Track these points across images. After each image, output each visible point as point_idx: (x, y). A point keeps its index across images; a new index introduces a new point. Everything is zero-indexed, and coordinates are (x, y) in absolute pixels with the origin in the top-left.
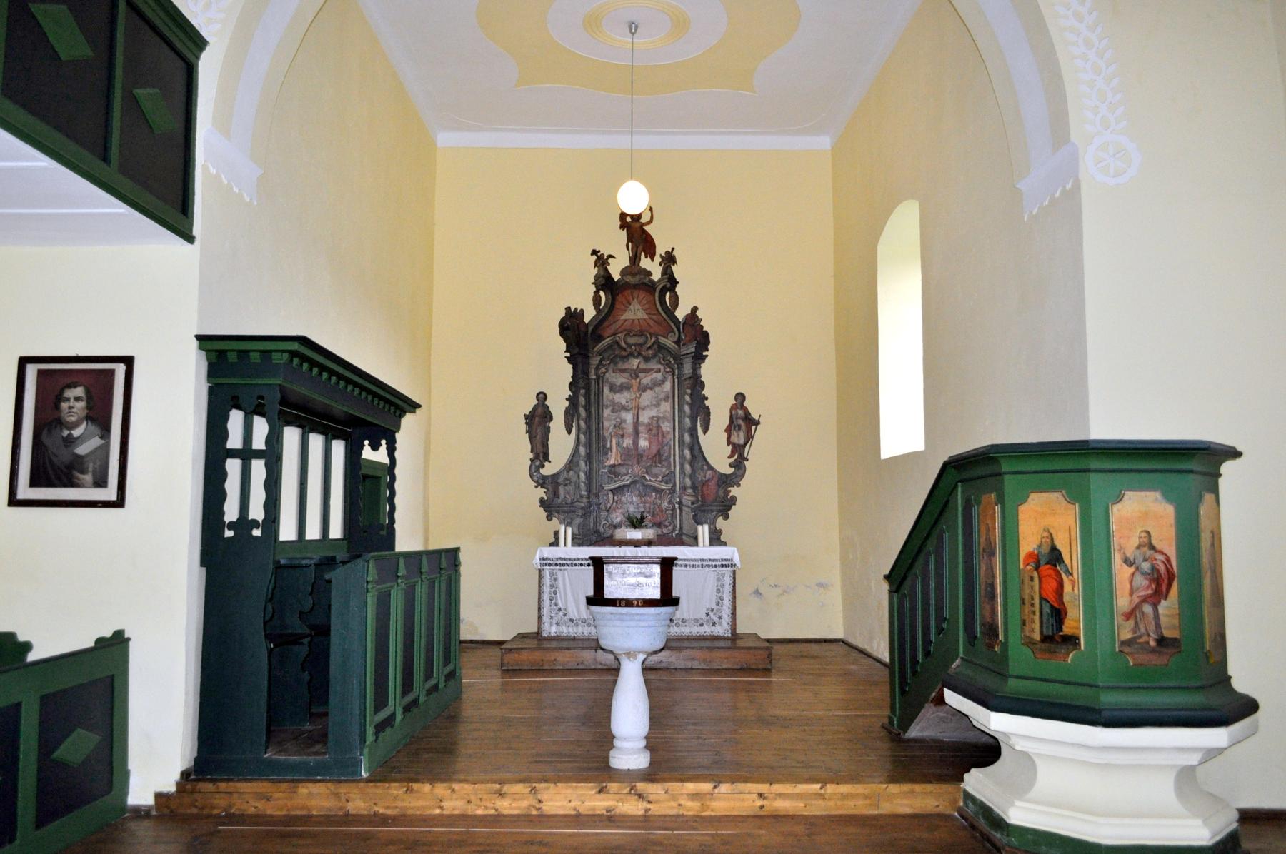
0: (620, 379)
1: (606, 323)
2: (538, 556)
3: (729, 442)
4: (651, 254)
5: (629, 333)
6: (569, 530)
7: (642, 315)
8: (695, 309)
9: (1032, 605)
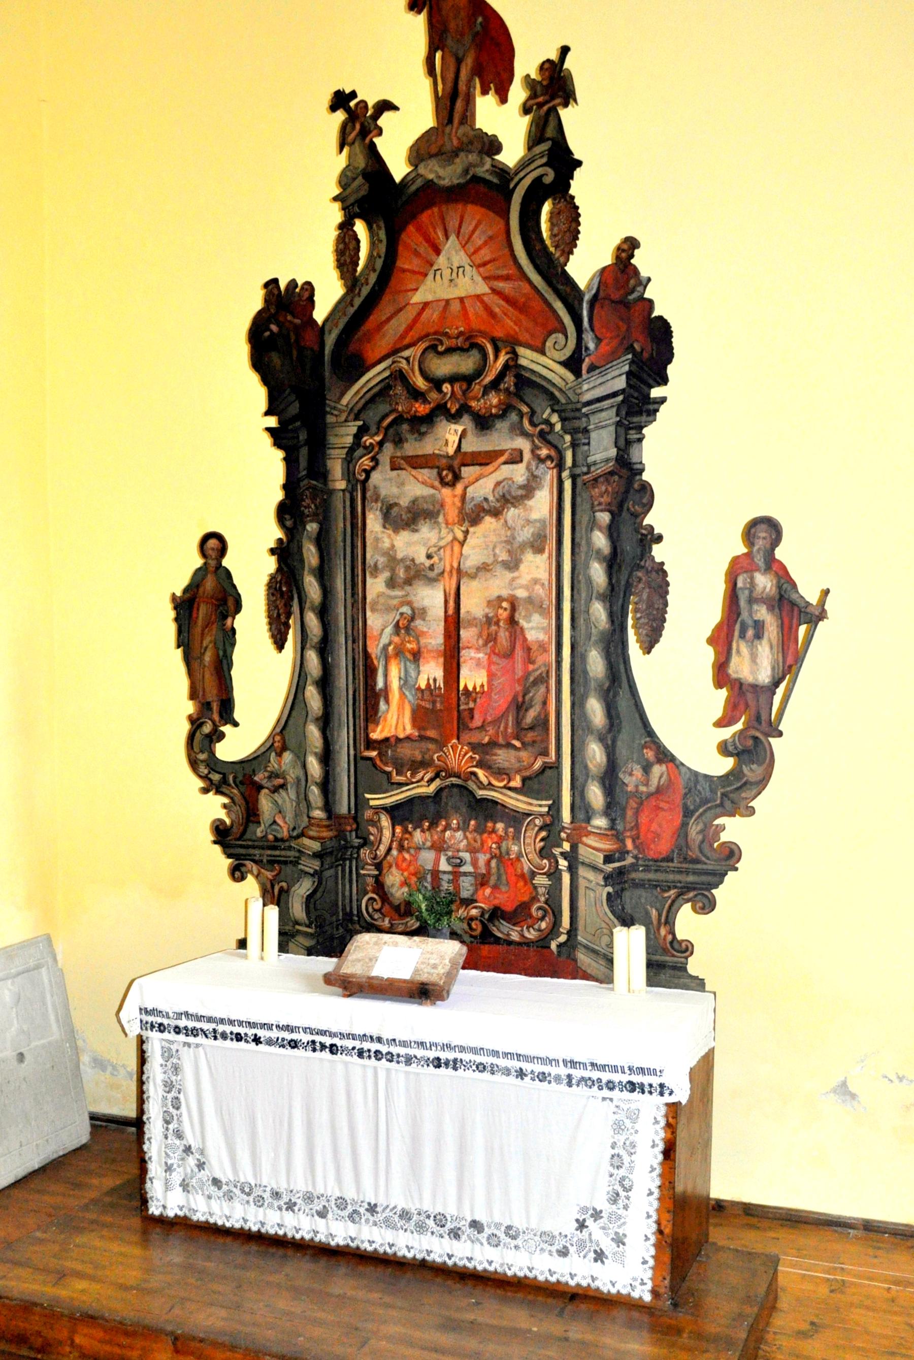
0: (413, 487)
3: (721, 676)
7: (471, 284)
8: (629, 246)
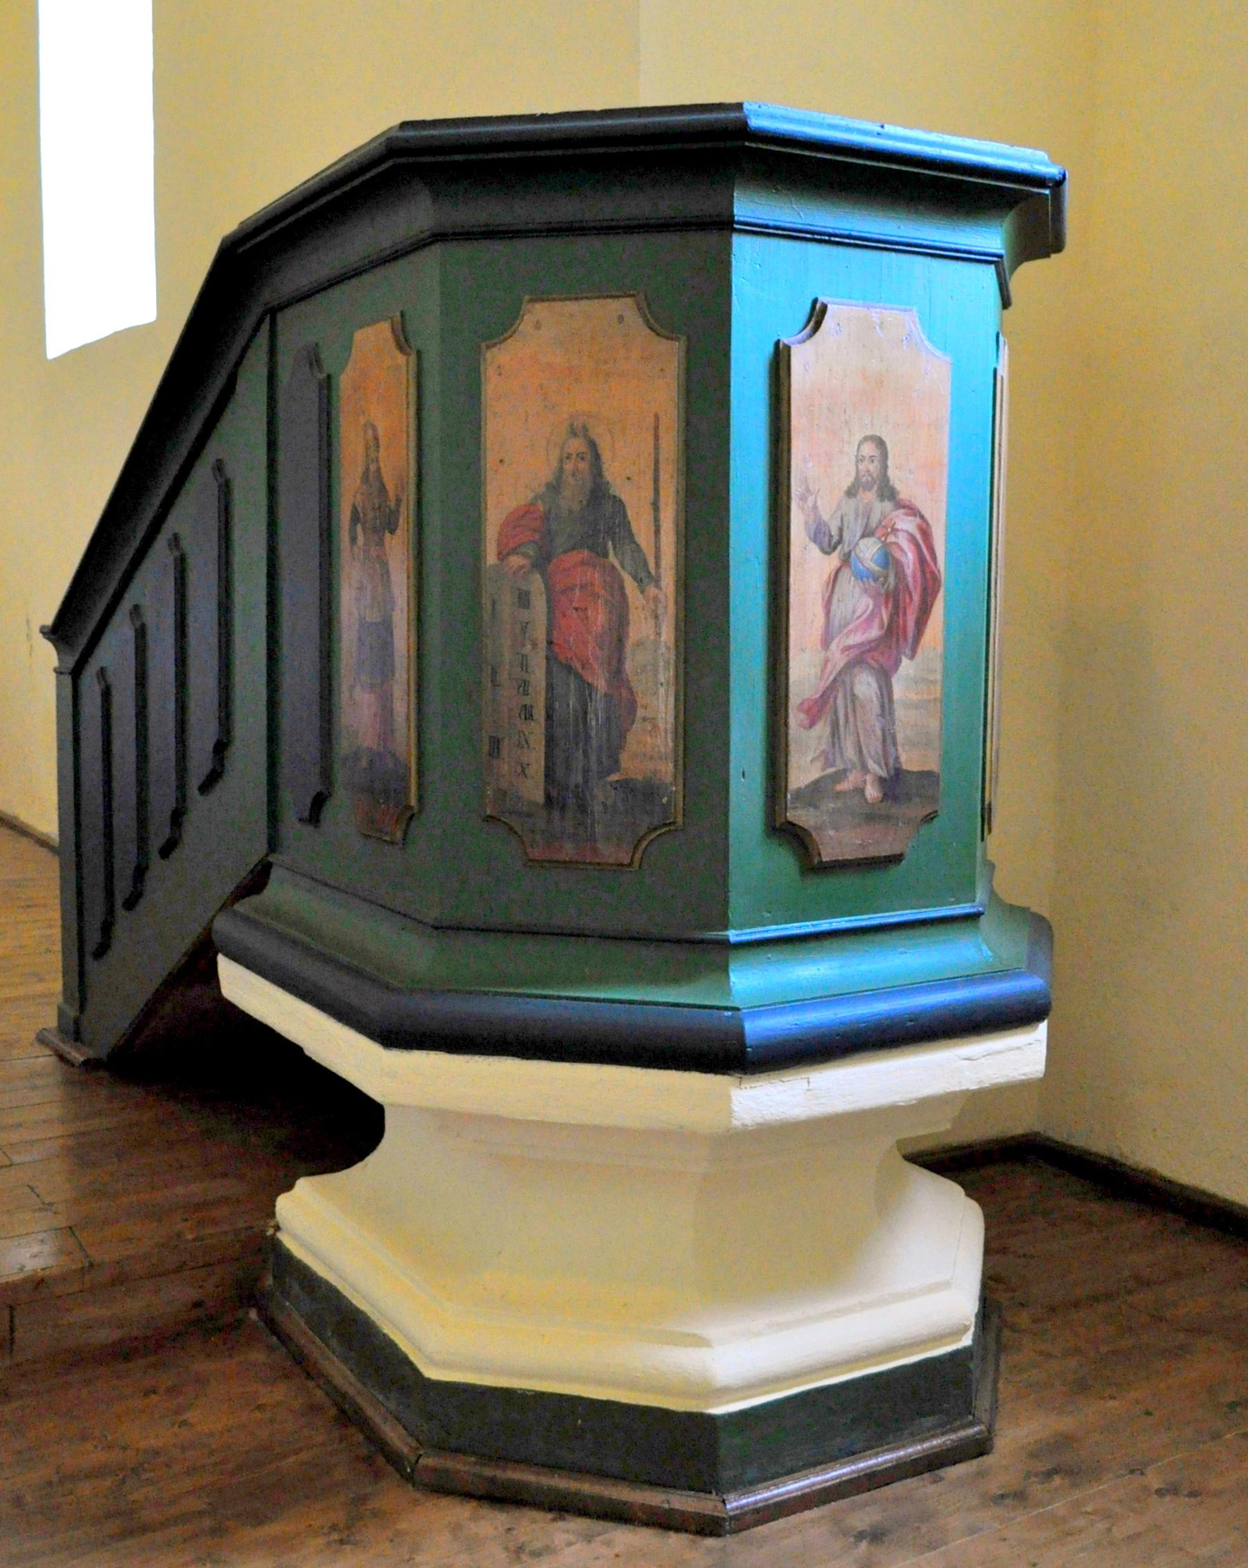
9: (524, 686)
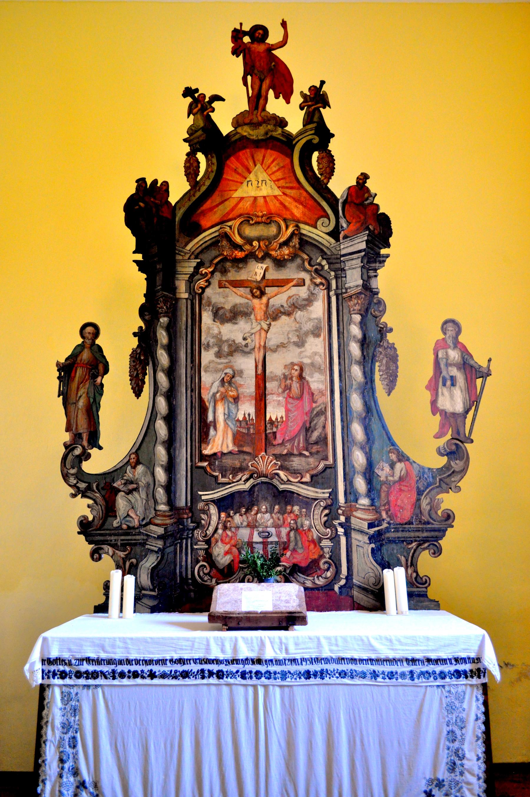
0: (234, 298)
1: (208, 205)
2: (36, 656)
3: (435, 409)
4: (285, 89)
5: (248, 219)
6: (130, 580)
